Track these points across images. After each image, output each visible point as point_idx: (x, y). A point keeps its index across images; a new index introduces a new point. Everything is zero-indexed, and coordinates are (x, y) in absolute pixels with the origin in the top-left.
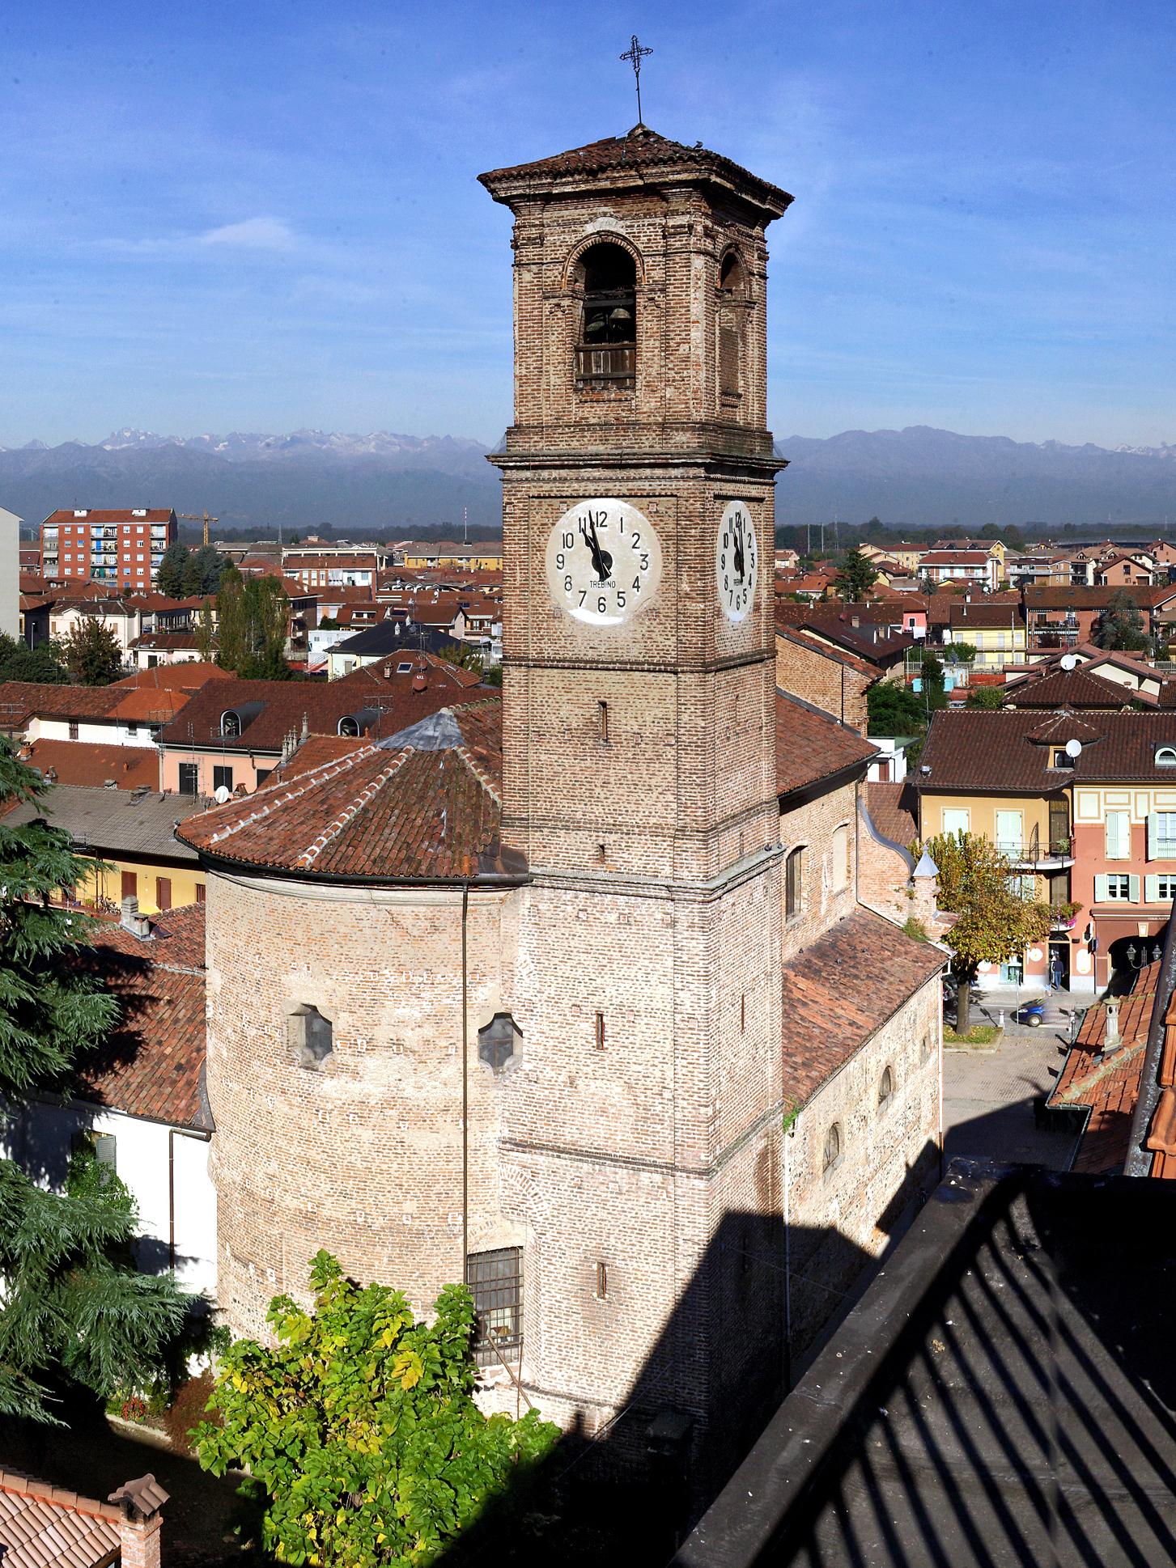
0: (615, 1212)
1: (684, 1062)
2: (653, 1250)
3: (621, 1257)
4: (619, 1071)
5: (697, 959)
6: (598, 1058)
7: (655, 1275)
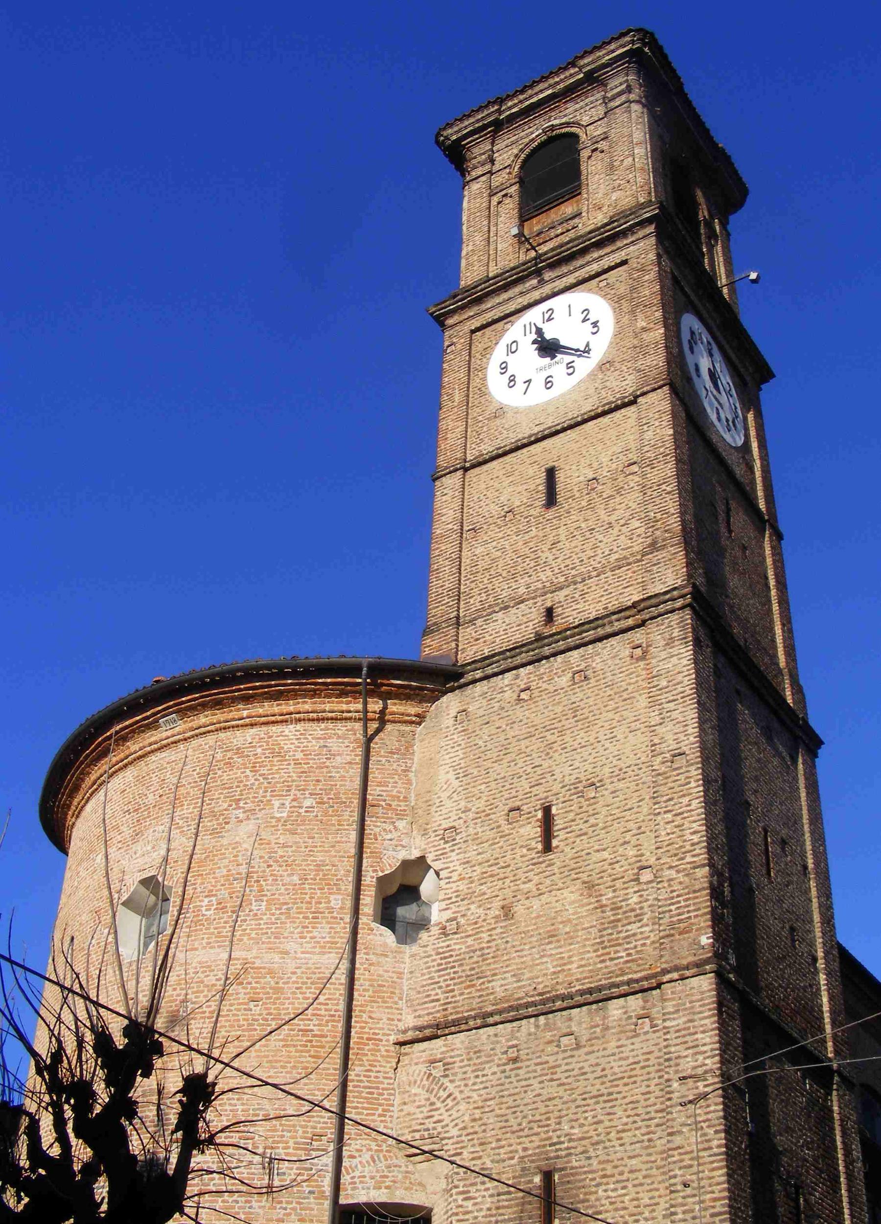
0: (569, 1080)
1: (669, 816)
2: (631, 1119)
3: (580, 1149)
4: (573, 871)
5: (680, 678)
6: (543, 865)
7: (634, 1162)
